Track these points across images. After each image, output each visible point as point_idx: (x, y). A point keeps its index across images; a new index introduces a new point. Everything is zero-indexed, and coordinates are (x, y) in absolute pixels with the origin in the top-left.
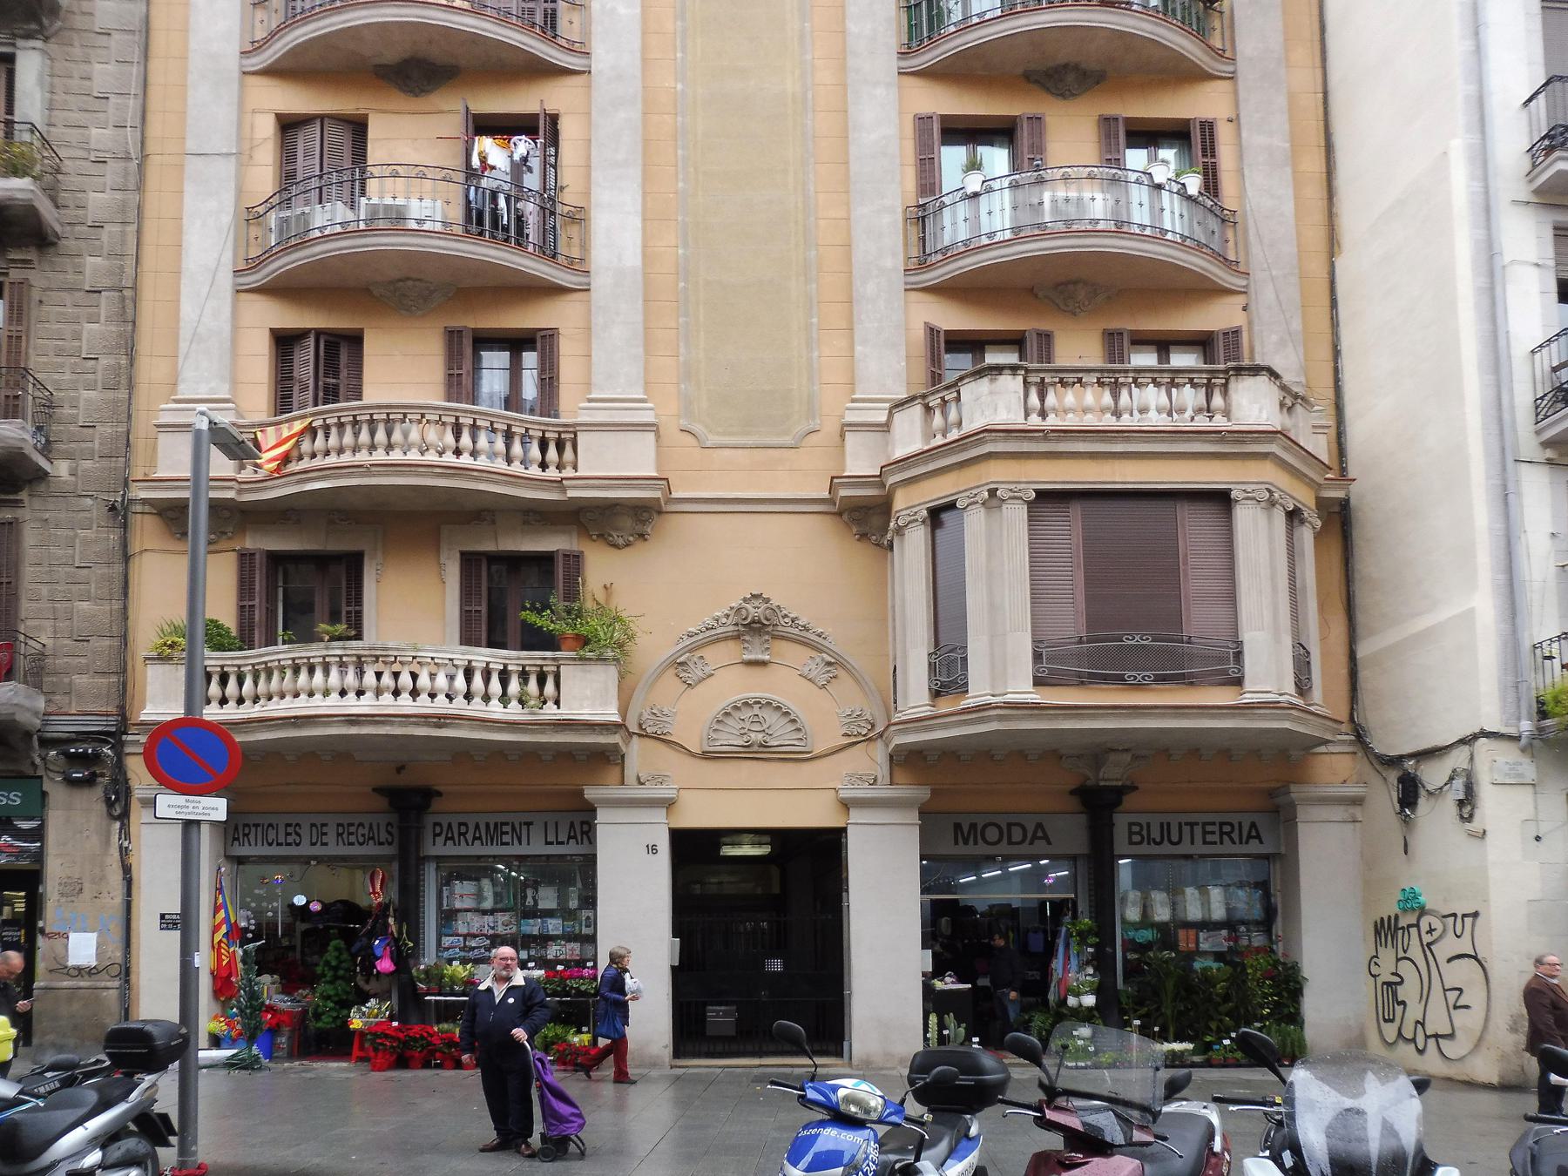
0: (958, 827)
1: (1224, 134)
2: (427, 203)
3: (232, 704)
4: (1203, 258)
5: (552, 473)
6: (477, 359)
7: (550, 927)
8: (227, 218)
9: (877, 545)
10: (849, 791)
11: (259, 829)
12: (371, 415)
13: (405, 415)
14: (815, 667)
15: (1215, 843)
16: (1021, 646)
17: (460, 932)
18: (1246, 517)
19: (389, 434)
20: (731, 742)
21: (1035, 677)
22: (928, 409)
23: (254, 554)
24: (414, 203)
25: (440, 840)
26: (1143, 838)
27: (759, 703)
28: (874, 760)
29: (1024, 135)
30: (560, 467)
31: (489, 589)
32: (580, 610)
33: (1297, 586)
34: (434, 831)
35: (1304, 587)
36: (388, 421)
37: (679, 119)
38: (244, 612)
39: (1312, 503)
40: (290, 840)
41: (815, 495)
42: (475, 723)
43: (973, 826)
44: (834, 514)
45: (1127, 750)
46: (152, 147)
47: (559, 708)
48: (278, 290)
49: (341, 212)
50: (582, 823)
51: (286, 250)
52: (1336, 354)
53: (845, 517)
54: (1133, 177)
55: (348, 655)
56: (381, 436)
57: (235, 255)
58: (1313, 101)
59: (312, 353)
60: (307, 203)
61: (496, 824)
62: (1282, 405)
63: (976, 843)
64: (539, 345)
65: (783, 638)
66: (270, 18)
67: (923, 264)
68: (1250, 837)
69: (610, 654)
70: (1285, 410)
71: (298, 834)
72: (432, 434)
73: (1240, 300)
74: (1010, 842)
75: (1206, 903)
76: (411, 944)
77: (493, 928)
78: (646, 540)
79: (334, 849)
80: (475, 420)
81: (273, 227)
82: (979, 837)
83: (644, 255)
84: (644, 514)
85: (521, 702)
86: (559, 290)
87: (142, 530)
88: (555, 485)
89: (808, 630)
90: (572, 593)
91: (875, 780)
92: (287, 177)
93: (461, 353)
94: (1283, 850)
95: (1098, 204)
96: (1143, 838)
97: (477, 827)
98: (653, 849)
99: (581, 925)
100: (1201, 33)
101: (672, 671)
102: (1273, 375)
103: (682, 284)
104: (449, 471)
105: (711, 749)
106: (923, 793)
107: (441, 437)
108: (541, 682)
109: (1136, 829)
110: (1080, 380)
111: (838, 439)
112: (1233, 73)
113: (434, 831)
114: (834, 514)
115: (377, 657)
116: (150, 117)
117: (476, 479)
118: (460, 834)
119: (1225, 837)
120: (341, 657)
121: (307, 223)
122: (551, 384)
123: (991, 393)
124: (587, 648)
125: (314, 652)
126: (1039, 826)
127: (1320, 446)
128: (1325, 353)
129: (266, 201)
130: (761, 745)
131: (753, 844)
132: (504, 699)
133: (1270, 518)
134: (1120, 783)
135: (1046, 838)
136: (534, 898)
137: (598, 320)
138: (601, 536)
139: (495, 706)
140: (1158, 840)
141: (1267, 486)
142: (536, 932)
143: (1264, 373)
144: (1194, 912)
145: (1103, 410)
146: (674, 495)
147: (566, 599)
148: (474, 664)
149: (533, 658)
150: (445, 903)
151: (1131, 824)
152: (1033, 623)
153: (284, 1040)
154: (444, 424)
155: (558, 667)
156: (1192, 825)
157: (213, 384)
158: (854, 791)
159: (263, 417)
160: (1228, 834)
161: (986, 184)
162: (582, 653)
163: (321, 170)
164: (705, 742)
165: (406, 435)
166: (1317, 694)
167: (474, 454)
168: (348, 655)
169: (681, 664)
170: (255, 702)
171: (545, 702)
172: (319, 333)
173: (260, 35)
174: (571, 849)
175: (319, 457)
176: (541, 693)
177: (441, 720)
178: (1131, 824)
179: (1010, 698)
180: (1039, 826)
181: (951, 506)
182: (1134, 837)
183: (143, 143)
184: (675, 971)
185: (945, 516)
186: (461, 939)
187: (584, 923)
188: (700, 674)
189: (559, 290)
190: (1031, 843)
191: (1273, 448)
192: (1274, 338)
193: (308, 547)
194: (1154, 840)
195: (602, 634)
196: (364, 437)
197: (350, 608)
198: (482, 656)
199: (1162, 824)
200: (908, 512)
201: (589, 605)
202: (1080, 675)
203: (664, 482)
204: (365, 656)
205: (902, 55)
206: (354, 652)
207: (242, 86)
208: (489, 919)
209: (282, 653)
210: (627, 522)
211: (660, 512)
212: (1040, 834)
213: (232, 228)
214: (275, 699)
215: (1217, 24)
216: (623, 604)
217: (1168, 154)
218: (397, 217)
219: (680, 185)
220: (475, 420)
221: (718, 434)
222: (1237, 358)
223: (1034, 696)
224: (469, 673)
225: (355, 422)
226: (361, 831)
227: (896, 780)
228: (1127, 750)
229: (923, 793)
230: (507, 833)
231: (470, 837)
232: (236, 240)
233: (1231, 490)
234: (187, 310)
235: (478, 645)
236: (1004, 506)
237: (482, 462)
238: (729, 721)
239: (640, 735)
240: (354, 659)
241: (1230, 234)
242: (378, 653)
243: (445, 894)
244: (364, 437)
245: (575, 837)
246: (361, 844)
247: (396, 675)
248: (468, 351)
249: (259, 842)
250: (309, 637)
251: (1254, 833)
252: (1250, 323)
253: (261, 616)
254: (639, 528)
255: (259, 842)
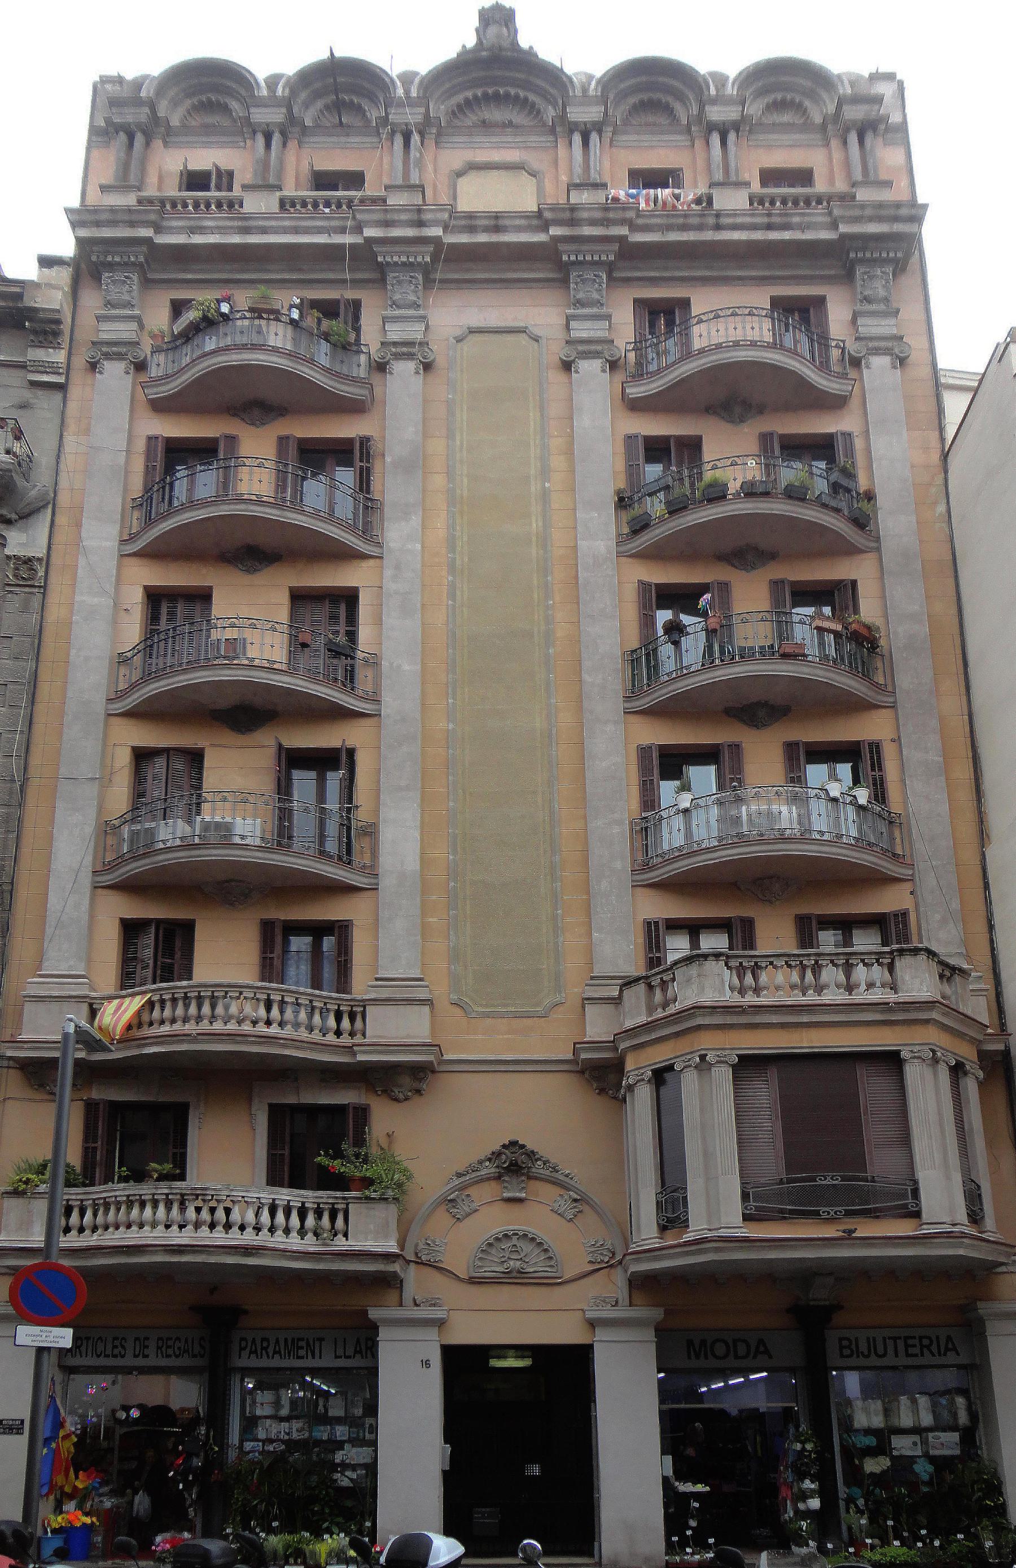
0: (690, 1343)
1: (889, 753)
2: (249, 821)
3: (74, 1232)
4: (875, 856)
5: (345, 1040)
6: (286, 943)
7: (338, 1434)
8: (89, 829)
9: (615, 1098)
10: (594, 1313)
11: (90, 1342)
12: (199, 992)
13: (226, 993)
14: (564, 1205)
15: (916, 1355)
16: (731, 1186)
17: (259, 1437)
18: (914, 1073)
19: (213, 1007)
20: (493, 1269)
21: (743, 1214)
22: (650, 987)
23: (98, 1104)
24: (239, 820)
25: (245, 1354)
26: (852, 1351)
27: (517, 1234)
28: (616, 1284)
29: (726, 755)
30: (352, 1034)
31: (292, 1136)
32: (366, 1155)
33: (966, 1128)
34: (240, 1345)
35: (971, 1130)
36: (213, 997)
37: (450, 751)
38: (88, 1155)
39: (974, 1057)
40: (116, 1351)
41: (561, 1057)
42: (275, 1252)
43: (703, 1342)
44: (577, 1072)
45: (831, 1274)
46: (32, 772)
47: (347, 1240)
48: (130, 887)
49: (182, 828)
50: (367, 1339)
51: (135, 858)
52: (991, 927)
53: (587, 1075)
54: (812, 793)
55: (173, 1194)
56: (206, 1009)
57: (95, 858)
58: (958, 724)
59: (153, 938)
60: (154, 819)
61: (293, 1340)
62: (941, 976)
63: (706, 1358)
64: (336, 931)
65: (536, 1178)
66: (131, 673)
67: (647, 867)
68: (947, 1349)
69: (390, 1193)
70: (945, 980)
71: (123, 1347)
72: (248, 1009)
73: (907, 887)
74: (737, 1357)
75: (916, 1411)
76: (217, 1449)
77: (288, 1434)
78: (422, 1095)
79: (153, 1361)
80: (283, 996)
81: (126, 837)
82: (709, 1353)
83: (422, 859)
84: (421, 1074)
85: (316, 1234)
86: (351, 889)
87: (6, 1086)
88: (347, 1050)
89: (557, 1172)
90: (360, 1140)
91: (617, 1302)
92: (138, 793)
93: (273, 941)
94: (978, 1361)
95: (787, 815)
96: (852, 1351)
97: (277, 1341)
98: (426, 1364)
99: (364, 1432)
100: (866, 673)
101: (442, 1210)
102: (931, 953)
103: (452, 884)
104: (263, 1040)
105: (477, 1275)
106: (657, 1314)
107: (256, 1010)
108: (333, 1218)
109: (845, 1343)
110: (771, 963)
111: (580, 1009)
112: (893, 703)
113: (240, 1345)
114: (577, 1072)
115: (197, 1195)
116: (33, 749)
117: (284, 1046)
118: (263, 1348)
119: (925, 1350)
120: (167, 1195)
121: (153, 835)
122: (346, 965)
123: (699, 975)
124: (372, 1189)
125: (145, 1190)
126: (761, 1342)
127: (979, 1009)
128: (981, 927)
129: (121, 816)
130: (519, 1272)
131: (516, 1357)
132: (302, 1232)
133: (935, 1074)
134: (827, 1303)
135: (767, 1352)
136: (324, 1406)
137: (384, 914)
138: (384, 1091)
139: (293, 1238)
140: (866, 1353)
141: (931, 1047)
142: (325, 1437)
143: (922, 953)
144: (906, 1420)
145: (793, 987)
146: (445, 1057)
147: (355, 1145)
148: (277, 1202)
149: (325, 1196)
150: (248, 1409)
151: (841, 1339)
152: (741, 1171)
153: (100, 1539)
154: (258, 999)
155: (347, 1204)
156: (895, 1339)
157: (72, 963)
158: (597, 1312)
159: (111, 991)
160: (928, 1347)
161: (694, 802)
162: (367, 1192)
163: (166, 795)
164: (471, 1269)
165: (227, 1008)
166: (989, 1223)
167: (281, 1024)
168: (173, 1194)
169: (451, 1201)
170: (93, 1232)
171: (335, 1235)
172: (159, 922)
173: (122, 686)
174: (357, 1362)
175: (155, 1025)
176: (333, 1227)
177: (247, 1250)
178: (841, 1339)
179: (723, 1232)
180: (761, 1342)
181: (670, 1068)
182: (844, 1350)
183: (25, 769)
184: (445, 1474)
185: (668, 1076)
186: (260, 1444)
187: (367, 1430)
188: (467, 1209)
189: (351, 889)
190: (755, 1357)
191: (935, 1015)
192: (938, 917)
193: (143, 1099)
194: (862, 1353)
195: (384, 1176)
196: (193, 1010)
197: (175, 1151)
198: (284, 1195)
199: (868, 1339)
200: (637, 1072)
201: (374, 1151)
202: (782, 1211)
203: (437, 1048)
204: (188, 1194)
205: (627, 698)
206: (178, 1191)
207: (106, 725)
208: (285, 1425)
209: (119, 1190)
210: (406, 1081)
211: (433, 1072)
212: (762, 1349)
213: (93, 839)
214: (111, 1230)
215: (879, 664)
216: (402, 1152)
217: (844, 770)
218: (225, 829)
219: (451, 804)
220: (283, 996)
221: (481, 1005)
222: (907, 939)
223: (744, 1230)
224: (273, 1211)
225: (186, 997)
226: (177, 1344)
227: (634, 1302)
228: (831, 1274)
229: (657, 1314)
230: (302, 1348)
231: (271, 1351)
232: (95, 847)
233: (900, 1051)
234: (54, 901)
235: (282, 1186)
236: (713, 1069)
237: (288, 1032)
238: (493, 1251)
239: (417, 1263)
240: (178, 1197)
241: (897, 833)
242: (198, 1192)
243: (248, 1402)
244: (193, 1010)
245: (360, 1352)
246: (177, 1356)
247: (212, 1210)
248: (279, 939)
249: (90, 1353)
250: (139, 1176)
251: (950, 1346)
252: (917, 905)
253: (101, 1157)
254: (416, 1085)
255: (90, 1353)
